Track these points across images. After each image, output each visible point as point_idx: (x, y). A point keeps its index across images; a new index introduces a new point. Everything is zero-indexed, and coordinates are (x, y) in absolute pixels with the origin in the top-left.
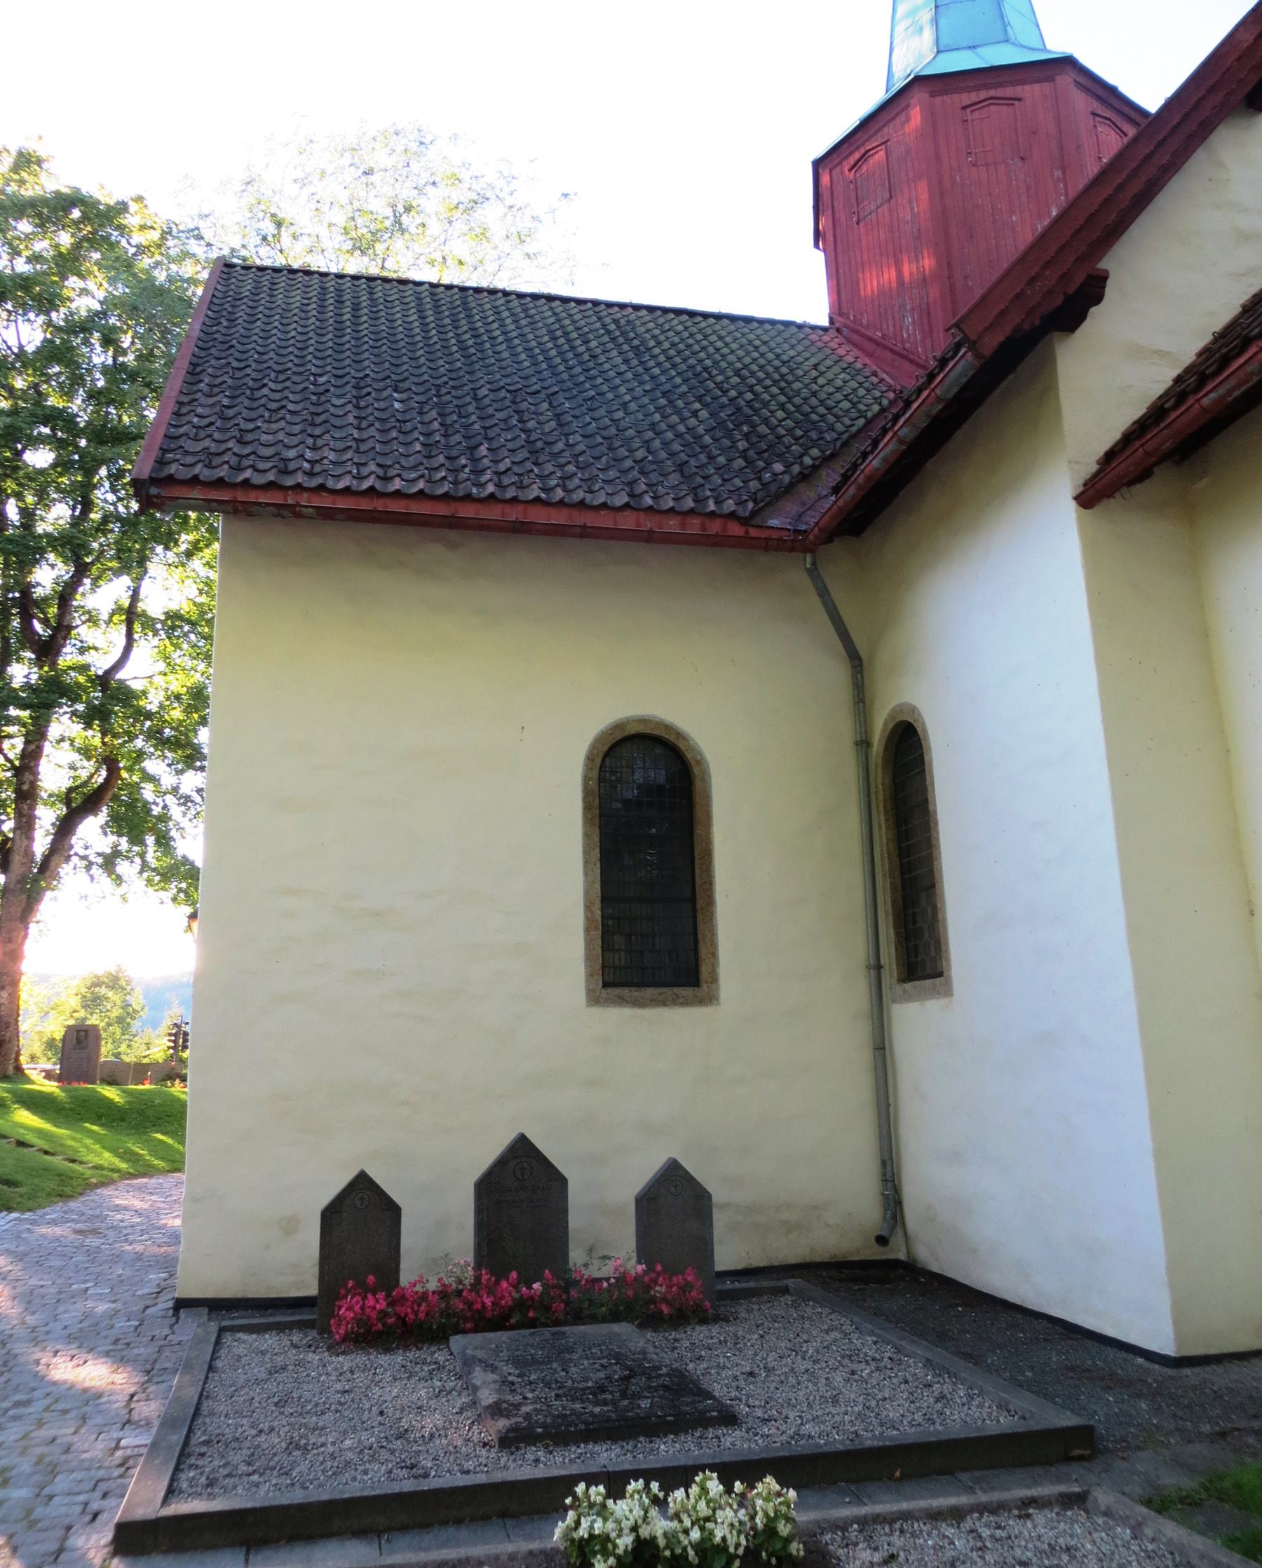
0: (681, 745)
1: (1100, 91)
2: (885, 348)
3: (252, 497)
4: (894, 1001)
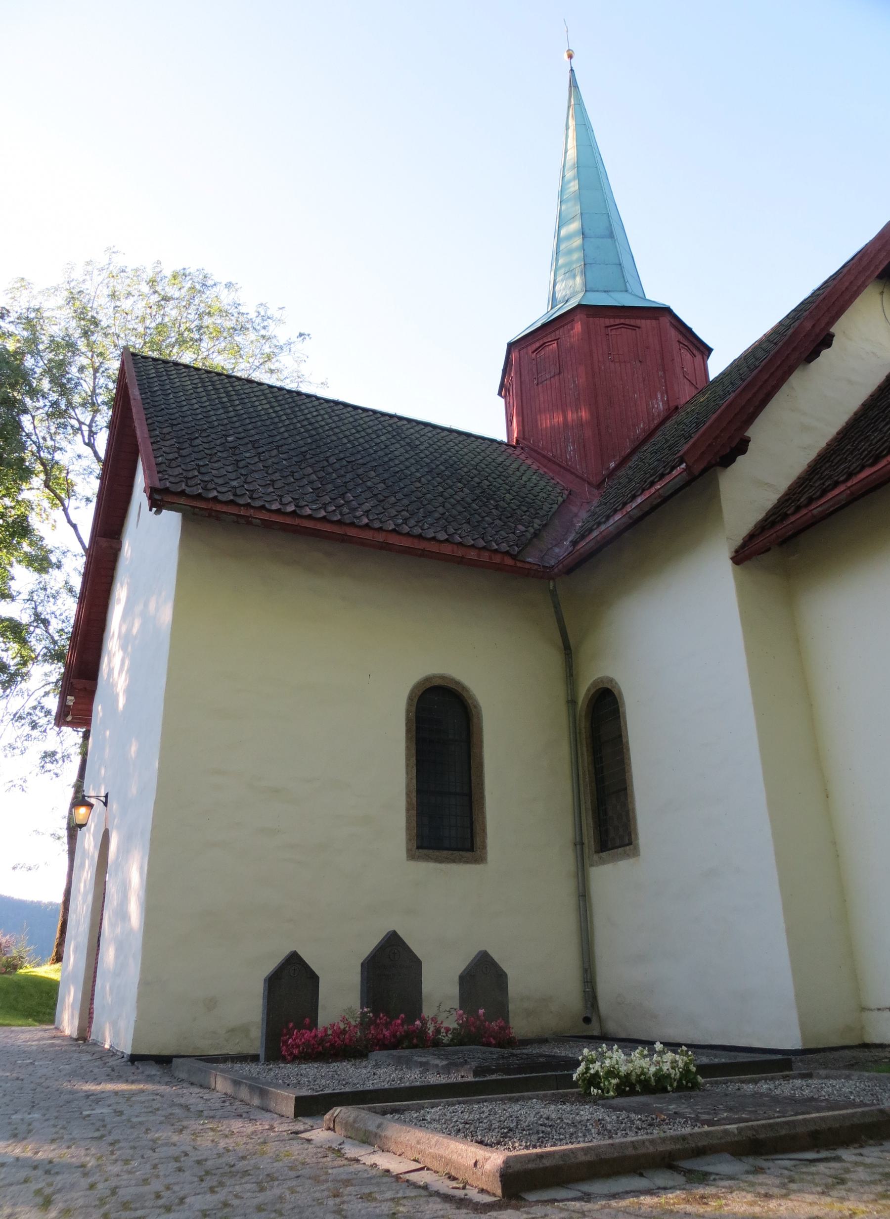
0: (465, 694)
1: (684, 331)
2: (555, 463)
3: (219, 507)
4: (592, 865)
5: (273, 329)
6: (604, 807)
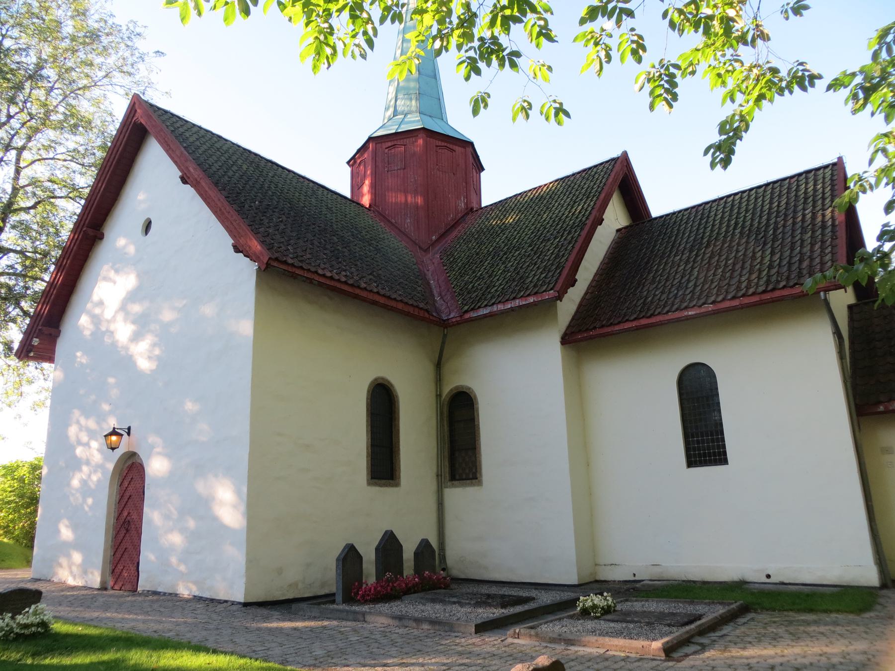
5: (138, 43)
6: (460, 457)
